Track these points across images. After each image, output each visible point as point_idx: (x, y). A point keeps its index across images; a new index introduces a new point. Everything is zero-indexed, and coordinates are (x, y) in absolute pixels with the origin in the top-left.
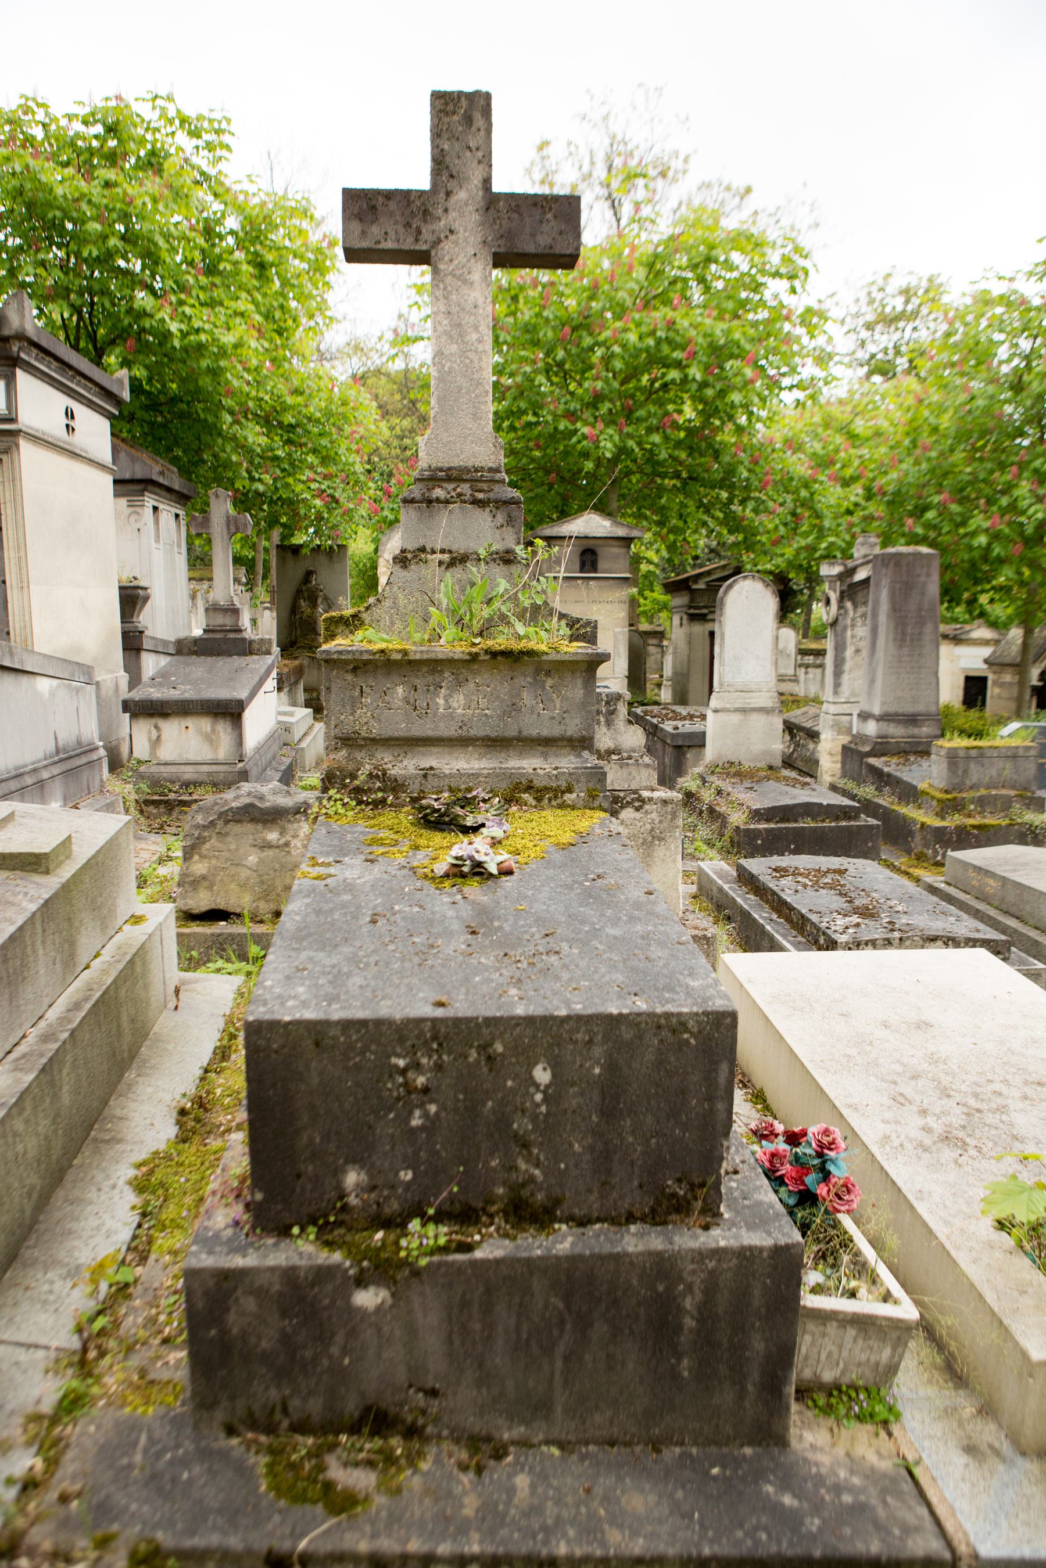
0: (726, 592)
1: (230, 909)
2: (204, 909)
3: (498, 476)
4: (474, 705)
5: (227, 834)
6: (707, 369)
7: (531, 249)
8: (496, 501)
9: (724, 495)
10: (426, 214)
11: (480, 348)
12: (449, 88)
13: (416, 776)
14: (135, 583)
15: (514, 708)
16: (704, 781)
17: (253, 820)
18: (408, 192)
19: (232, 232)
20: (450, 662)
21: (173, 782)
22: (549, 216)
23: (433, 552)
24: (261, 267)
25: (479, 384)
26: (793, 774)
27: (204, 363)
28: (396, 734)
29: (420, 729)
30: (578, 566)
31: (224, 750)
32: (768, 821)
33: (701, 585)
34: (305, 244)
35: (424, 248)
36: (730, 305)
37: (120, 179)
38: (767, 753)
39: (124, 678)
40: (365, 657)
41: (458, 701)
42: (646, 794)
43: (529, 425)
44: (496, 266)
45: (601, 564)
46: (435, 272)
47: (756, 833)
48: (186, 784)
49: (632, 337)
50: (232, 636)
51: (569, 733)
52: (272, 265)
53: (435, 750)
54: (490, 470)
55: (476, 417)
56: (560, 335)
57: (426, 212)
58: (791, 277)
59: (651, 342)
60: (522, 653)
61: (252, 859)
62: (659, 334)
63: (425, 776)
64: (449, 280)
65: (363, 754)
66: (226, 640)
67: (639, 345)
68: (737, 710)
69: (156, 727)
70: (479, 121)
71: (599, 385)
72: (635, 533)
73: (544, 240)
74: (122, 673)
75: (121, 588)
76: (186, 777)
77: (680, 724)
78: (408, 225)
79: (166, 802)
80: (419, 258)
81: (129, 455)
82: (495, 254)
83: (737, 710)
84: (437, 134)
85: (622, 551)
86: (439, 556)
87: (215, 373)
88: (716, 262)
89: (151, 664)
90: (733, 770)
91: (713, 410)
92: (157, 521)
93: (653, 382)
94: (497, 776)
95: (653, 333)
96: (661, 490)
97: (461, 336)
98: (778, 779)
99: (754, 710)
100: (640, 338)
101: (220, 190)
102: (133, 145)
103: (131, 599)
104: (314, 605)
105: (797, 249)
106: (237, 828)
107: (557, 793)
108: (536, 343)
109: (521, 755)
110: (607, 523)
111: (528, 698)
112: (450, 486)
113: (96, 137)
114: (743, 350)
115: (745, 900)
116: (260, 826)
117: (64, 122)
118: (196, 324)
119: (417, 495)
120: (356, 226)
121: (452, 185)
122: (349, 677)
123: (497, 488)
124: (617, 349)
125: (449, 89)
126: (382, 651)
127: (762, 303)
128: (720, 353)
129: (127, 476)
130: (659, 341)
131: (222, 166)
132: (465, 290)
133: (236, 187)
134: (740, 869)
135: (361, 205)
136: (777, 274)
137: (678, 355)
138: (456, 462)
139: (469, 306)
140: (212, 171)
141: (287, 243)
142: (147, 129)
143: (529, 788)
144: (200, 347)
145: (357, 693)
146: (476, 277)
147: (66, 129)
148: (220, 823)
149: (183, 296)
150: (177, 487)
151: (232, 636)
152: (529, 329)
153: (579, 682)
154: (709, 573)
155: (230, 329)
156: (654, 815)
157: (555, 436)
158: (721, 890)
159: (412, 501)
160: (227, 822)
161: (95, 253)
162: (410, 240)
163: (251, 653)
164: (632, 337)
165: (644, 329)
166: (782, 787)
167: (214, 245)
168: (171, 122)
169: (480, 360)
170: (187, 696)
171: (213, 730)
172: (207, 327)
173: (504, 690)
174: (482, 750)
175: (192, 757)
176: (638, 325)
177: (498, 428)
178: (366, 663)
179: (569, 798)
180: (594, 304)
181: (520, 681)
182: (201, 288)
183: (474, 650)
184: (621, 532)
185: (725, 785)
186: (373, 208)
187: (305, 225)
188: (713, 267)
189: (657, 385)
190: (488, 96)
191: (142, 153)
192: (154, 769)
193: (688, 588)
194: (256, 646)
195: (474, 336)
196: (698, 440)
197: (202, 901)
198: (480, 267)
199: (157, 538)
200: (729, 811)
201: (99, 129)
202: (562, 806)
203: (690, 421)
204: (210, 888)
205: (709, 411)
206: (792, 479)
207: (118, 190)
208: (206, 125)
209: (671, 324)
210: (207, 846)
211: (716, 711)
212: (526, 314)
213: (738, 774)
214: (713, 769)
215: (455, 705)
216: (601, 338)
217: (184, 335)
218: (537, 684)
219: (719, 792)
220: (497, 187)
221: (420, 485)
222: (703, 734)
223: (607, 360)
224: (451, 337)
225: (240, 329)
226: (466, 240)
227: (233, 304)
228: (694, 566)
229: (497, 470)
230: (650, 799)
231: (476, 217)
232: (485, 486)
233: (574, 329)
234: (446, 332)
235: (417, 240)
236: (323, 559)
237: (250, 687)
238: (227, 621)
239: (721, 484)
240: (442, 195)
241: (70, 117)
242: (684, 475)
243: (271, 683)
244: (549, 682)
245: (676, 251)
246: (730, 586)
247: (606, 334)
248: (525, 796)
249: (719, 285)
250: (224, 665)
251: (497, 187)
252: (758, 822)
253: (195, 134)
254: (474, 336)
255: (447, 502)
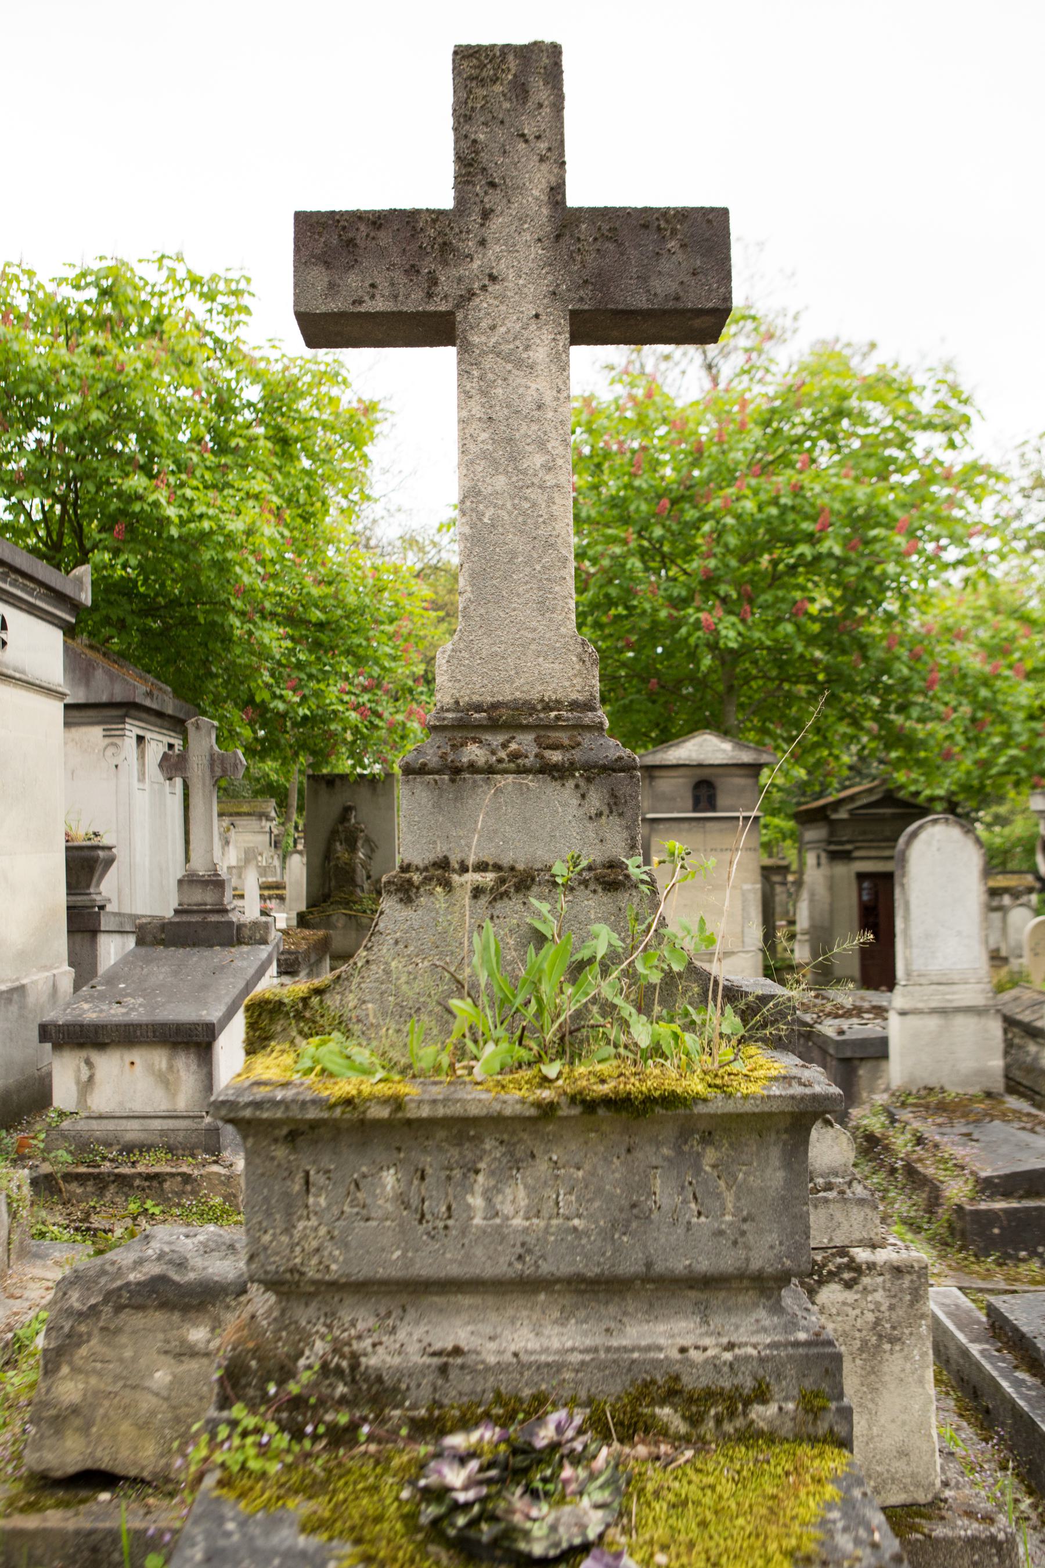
0: (908, 843)
1: (119, 1470)
2: (71, 1470)
3: (588, 718)
4: (548, 1207)
5: (118, 1331)
6: (848, 543)
7: (641, 302)
8: (587, 767)
9: (876, 701)
10: (446, 250)
11: (550, 479)
12: (485, 40)
13: (424, 1369)
14: (94, 842)
15: (634, 1214)
16: (893, 1120)
17: (165, 1305)
18: (413, 215)
19: (250, 405)
20: (495, 1122)
21: (108, 1145)
22: (672, 244)
23: (464, 869)
24: (283, 442)
25: (549, 545)
26: (1024, 1106)
27: (207, 554)
28: (381, 1273)
29: (427, 1264)
30: (690, 803)
31: (185, 1095)
32: (1007, 1195)
33: (843, 814)
34: (337, 415)
35: (443, 308)
36: (872, 464)
37: (111, 344)
38: (980, 1073)
39: (66, 974)
40: (312, 1114)
41: (515, 1201)
42: (862, 1255)
43: (618, 617)
44: (577, 339)
45: (721, 800)
46: (465, 349)
47: (991, 1216)
48: (129, 1149)
49: (749, 505)
50: (214, 918)
51: (755, 1265)
52: (296, 441)
53: (466, 1300)
54: (574, 705)
55: (544, 607)
56: (654, 508)
57: (446, 247)
58: (947, 428)
59: (774, 511)
60: (649, 1101)
61: (161, 1377)
62: (783, 501)
63: (443, 1370)
64: (488, 361)
65: (311, 1311)
66: (205, 924)
67: (759, 516)
68: (934, 1011)
69: (88, 1063)
70: (540, 92)
71: (712, 563)
72: (765, 758)
73: (668, 283)
74: (66, 968)
75: (68, 849)
76: (129, 1137)
77: (845, 1024)
78: (413, 270)
79: (97, 1177)
80: (433, 329)
81: (107, 672)
82: (574, 314)
83: (934, 1011)
84: (464, 115)
85: (749, 781)
86: (472, 878)
87: (222, 567)
88: (849, 415)
89: (112, 950)
90: (933, 1100)
91: (860, 591)
92: (142, 756)
93: (775, 563)
94: (602, 1366)
95: (775, 502)
96: (791, 698)
97: (513, 459)
98: (1004, 1117)
99: (958, 1010)
100: (760, 509)
101: (235, 357)
102: (130, 309)
103: (85, 864)
104: (353, 848)
105: (954, 390)
106: (136, 1320)
107: (736, 1401)
108: (625, 520)
109: (651, 1312)
110: (727, 746)
111: (664, 1192)
112: (496, 739)
113: (88, 302)
114: (896, 520)
115: (1018, 1384)
116: (176, 1317)
117: (50, 288)
118: (198, 510)
119: (431, 758)
120: (320, 277)
121: (492, 199)
122: (280, 1152)
123: (587, 739)
124: (729, 521)
125: (486, 42)
126: (348, 1102)
127: (914, 462)
128: (862, 522)
129: (104, 699)
130: (784, 510)
131: (240, 331)
132: (518, 378)
133: (257, 354)
134: (992, 1311)
135: (328, 240)
136: (929, 426)
137: (807, 526)
138: (507, 693)
139: (527, 406)
140: (228, 338)
141: (316, 414)
142: (152, 294)
143: (672, 1393)
144: (204, 537)
145: (297, 1187)
146: (540, 354)
147: (51, 296)
148: (108, 1309)
149: (184, 477)
150: (170, 711)
151: (214, 918)
152: (614, 502)
153: (775, 1154)
154: (852, 798)
155: (246, 517)
156: (879, 1296)
157: (654, 632)
158: (965, 1353)
159: (422, 770)
160: (119, 1309)
161: (73, 429)
162: (418, 295)
163: (240, 942)
164: (749, 505)
165: (763, 497)
166: (1012, 1131)
167: (227, 420)
168: (180, 284)
169: (551, 501)
170: (134, 1017)
171: (170, 1067)
172: (211, 512)
173: (614, 1174)
174: (567, 1300)
175: (138, 1106)
176: (756, 493)
177: (580, 626)
178: (315, 1125)
179: (762, 1414)
180: (696, 473)
181: (647, 1155)
182: (208, 468)
183: (546, 1094)
184: (746, 757)
185: (927, 1128)
186: (351, 243)
187: (335, 392)
188: (845, 423)
189: (781, 567)
190: (555, 50)
191: (147, 321)
192: (82, 1125)
193: (826, 819)
194: (246, 932)
195: (539, 460)
196: (837, 633)
197: (70, 1454)
198: (547, 337)
199: (142, 778)
200: (941, 1175)
201: (92, 293)
202: (749, 1436)
203: (825, 609)
204: (85, 1430)
205: (853, 595)
206: (964, 676)
207: (108, 358)
208: (221, 286)
209: (797, 490)
210: (83, 1351)
211: (903, 1013)
212: (612, 486)
213: (942, 1107)
214: (903, 1099)
215: (508, 1209)
216: (709, 509)
217: (183, 522)
218: (685, 1160)
219: (920, 1141)
220: (574, 199)
221: (439, 739)
222: (884, 1042)
223: (720, 533)
224: (495, 463)
225: (251, 511)
226: (519, 291)
227: (245, 485)
228: (838, 791)
229: (587, 706)
230: (871, 1266)
231: (537, 251)
232: (564, 737)
233: (674, 502)
234: (485, 455)
235: (430, 295)
236: (364, 791)
237: (228, 1000)
238: (208, 897)
239: (873, 687)
240: (476, 217)
241: (60, 281)
242: (821, 677)
243: (273, 969)
244: (710, 1155)
245: (798, 405)
246: (914, 835)
247: (715, 504)
248: (665, 1412)
249: (856, 444)
250: (200, 960)
251: (574, 199)
252: (991, 1198)
253: (209, 297)
254: (539, 460)
255: (490, 770)
